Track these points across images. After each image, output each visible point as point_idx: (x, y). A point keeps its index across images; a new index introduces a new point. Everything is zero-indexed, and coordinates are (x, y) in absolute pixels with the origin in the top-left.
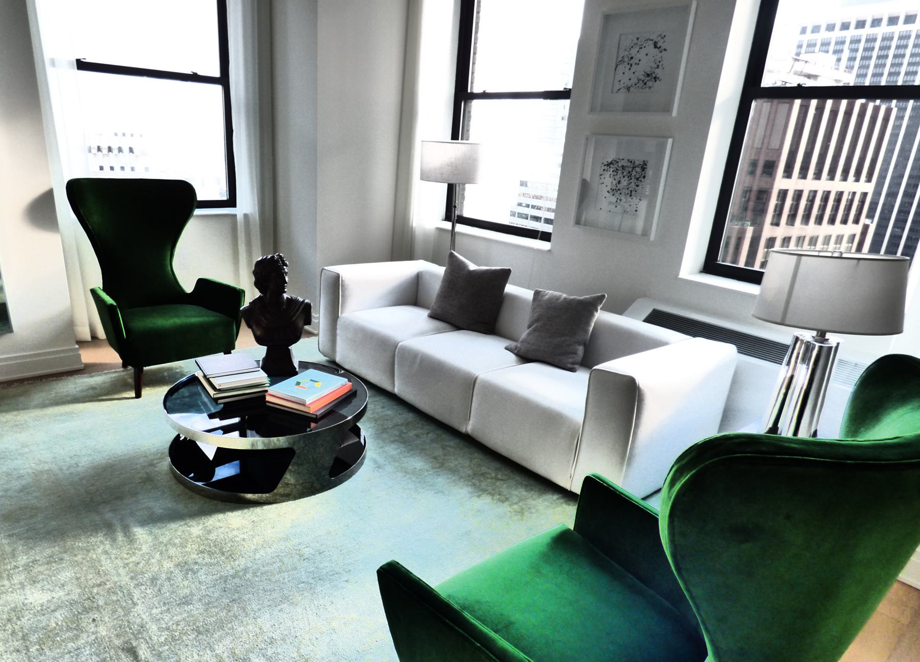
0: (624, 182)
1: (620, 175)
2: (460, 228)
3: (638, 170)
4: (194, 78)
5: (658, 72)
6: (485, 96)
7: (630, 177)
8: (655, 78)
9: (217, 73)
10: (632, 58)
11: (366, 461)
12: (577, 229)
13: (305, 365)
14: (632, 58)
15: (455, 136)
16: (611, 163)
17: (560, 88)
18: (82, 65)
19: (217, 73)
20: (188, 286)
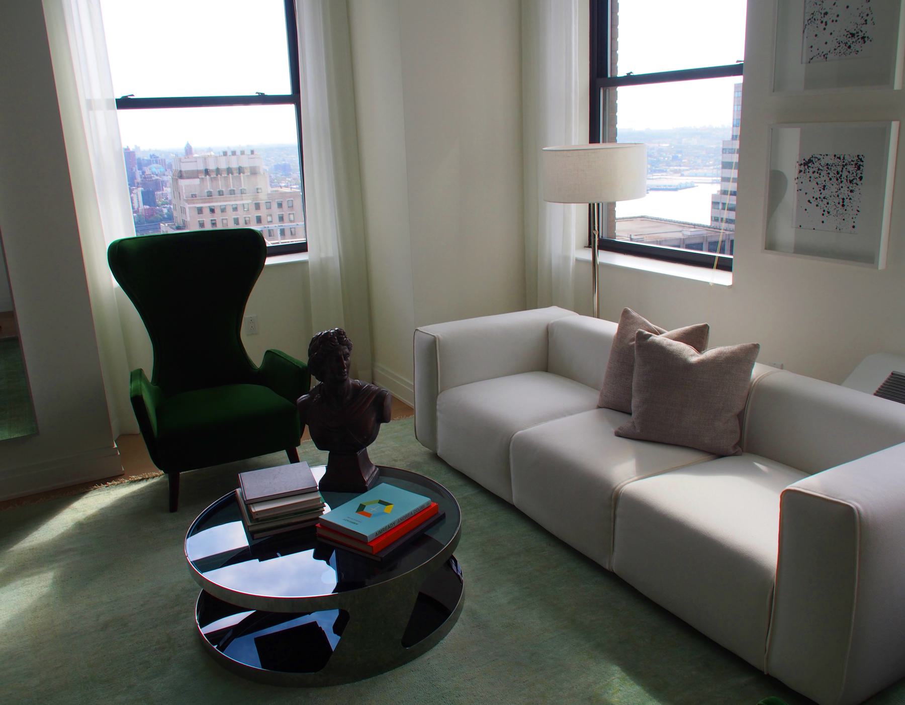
0: (832, 188)
1: (824, 177)
2: (606, 258)
3: (851, 168)
4: (262, 99)
5: (867, 30)
6: (631, 80)
7: (839, 178)
8: (863, 38)
9: (287, 91)
10: (826, 14)
11: (462, 616)
12: (771, 256)
13: (385, 473)
14: (826, 14)
15: (594, 137)
16: (810, 161)
17: (733, 62)
18: (125, 103)
19: (287, 91)
20: (257, 359)
